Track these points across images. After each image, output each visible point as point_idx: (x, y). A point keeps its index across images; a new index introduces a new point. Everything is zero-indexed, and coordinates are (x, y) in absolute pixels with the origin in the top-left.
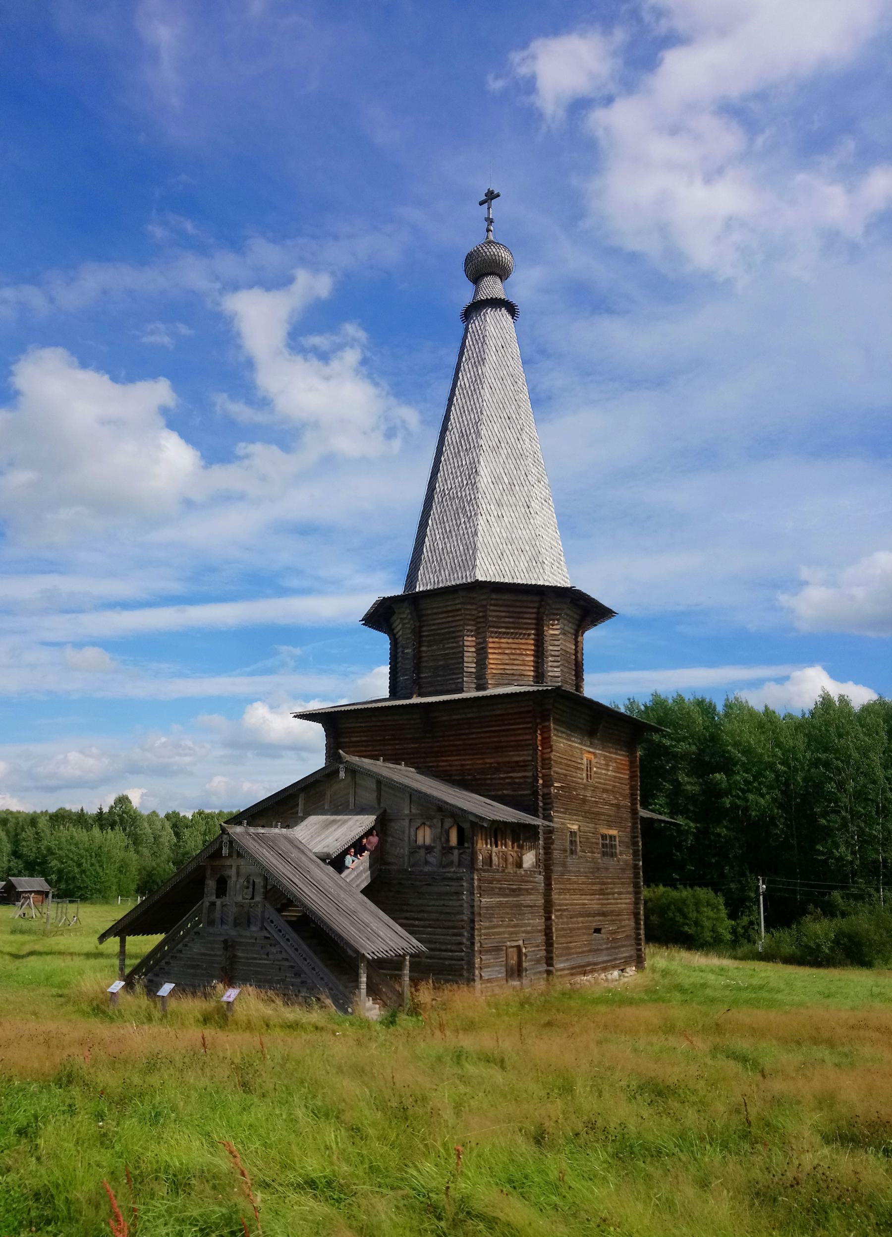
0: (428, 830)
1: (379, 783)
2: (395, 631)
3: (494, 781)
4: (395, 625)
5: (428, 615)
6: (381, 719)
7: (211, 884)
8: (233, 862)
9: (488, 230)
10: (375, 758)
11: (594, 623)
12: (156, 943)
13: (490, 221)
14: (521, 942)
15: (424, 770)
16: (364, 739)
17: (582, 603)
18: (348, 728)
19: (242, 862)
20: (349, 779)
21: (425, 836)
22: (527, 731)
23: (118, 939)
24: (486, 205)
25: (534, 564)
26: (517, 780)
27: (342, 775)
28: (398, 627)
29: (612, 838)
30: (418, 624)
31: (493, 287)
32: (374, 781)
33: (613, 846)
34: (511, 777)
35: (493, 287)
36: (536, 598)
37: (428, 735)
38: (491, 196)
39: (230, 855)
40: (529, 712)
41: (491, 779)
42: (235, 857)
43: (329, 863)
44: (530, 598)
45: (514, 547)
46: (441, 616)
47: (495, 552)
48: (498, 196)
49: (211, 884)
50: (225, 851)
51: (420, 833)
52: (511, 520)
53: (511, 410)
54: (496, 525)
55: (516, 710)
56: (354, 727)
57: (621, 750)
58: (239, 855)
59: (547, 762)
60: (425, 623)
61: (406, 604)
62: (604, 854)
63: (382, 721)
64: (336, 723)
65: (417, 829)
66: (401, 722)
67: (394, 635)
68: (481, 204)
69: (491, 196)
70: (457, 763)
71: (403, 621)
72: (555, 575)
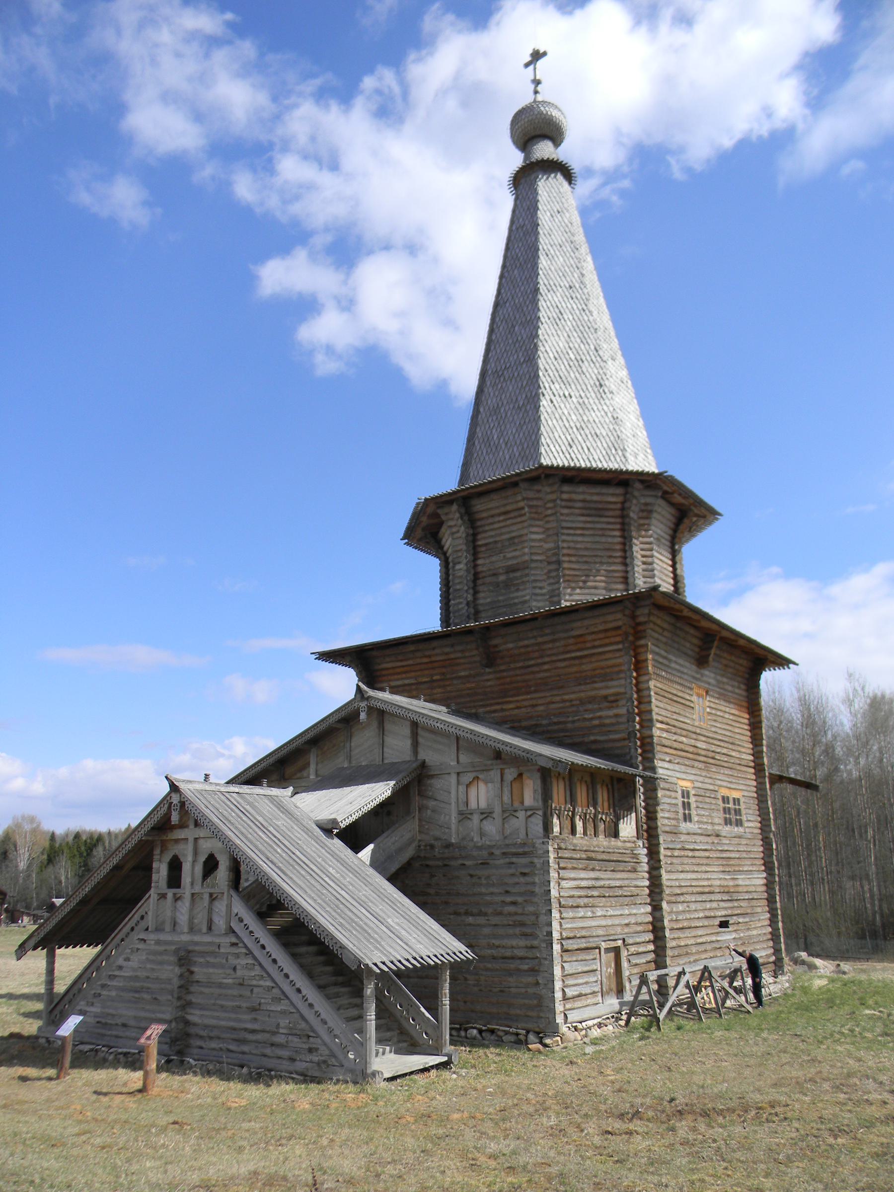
0: (482, 786)
1: (415, 725)
2: (445, 548)
3: (577, 724)
4: (444, 540)
5: (483, 519)
6: (427, 653)
7: (160, 871)
8: (189, 833)
9: (536, 92)
10: (417, 697)
11: (693, 530)
12: (85, 962)
13: (537, 82)
14: (620, 943)
15: (499, 724)
16: (407, 682)
17: (678, 499)
18: (387, 669)
19: (201, 833)
20: (375, 724)
21: (481, 795)
22: (618, 655)
23: (42, 953)
24: (532, 67)
25: (613, 451)
26: (607, 721)
27: (363, 716)
28: (448, 543)
29: (736, 801)
30: (471, 532)
31: (544, 150)
32: (408, 723)
33: (738, 812)
34: (600, 717)
35: (544, 150)
36: (620, 491)
37: (487, 670)
38: (537, 56)
39: (182, 826)
40: (618, 628)
41: (574, 722)
42: (192, 826)
43: (338, 836)
44: (611, 490)
45: (588, 432)
46: (497, 519)
47: (563, 437)
48: (545, 54)
49: (160, 871)
50: (175, 818)
51: (473, 792)
52: (581, 401)
53: (575, 279)
54: (562, 406)
55: (601, 628)
56: (393, 668)
57: (739, 688)
58: (197, 824)
59: (640, 628)
60: (481, 530)
61: (455, 507)
62: (727, 822)
63: (429, 656)
64: (365, 660)
65: (468, 786)
66: (452, 656)
67: (445, 554)
68: (527, 65)
69: (537, 56)
70: (526, 703)
71: (454, 536)
72: (641, 460)
